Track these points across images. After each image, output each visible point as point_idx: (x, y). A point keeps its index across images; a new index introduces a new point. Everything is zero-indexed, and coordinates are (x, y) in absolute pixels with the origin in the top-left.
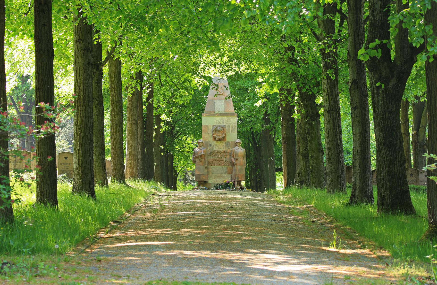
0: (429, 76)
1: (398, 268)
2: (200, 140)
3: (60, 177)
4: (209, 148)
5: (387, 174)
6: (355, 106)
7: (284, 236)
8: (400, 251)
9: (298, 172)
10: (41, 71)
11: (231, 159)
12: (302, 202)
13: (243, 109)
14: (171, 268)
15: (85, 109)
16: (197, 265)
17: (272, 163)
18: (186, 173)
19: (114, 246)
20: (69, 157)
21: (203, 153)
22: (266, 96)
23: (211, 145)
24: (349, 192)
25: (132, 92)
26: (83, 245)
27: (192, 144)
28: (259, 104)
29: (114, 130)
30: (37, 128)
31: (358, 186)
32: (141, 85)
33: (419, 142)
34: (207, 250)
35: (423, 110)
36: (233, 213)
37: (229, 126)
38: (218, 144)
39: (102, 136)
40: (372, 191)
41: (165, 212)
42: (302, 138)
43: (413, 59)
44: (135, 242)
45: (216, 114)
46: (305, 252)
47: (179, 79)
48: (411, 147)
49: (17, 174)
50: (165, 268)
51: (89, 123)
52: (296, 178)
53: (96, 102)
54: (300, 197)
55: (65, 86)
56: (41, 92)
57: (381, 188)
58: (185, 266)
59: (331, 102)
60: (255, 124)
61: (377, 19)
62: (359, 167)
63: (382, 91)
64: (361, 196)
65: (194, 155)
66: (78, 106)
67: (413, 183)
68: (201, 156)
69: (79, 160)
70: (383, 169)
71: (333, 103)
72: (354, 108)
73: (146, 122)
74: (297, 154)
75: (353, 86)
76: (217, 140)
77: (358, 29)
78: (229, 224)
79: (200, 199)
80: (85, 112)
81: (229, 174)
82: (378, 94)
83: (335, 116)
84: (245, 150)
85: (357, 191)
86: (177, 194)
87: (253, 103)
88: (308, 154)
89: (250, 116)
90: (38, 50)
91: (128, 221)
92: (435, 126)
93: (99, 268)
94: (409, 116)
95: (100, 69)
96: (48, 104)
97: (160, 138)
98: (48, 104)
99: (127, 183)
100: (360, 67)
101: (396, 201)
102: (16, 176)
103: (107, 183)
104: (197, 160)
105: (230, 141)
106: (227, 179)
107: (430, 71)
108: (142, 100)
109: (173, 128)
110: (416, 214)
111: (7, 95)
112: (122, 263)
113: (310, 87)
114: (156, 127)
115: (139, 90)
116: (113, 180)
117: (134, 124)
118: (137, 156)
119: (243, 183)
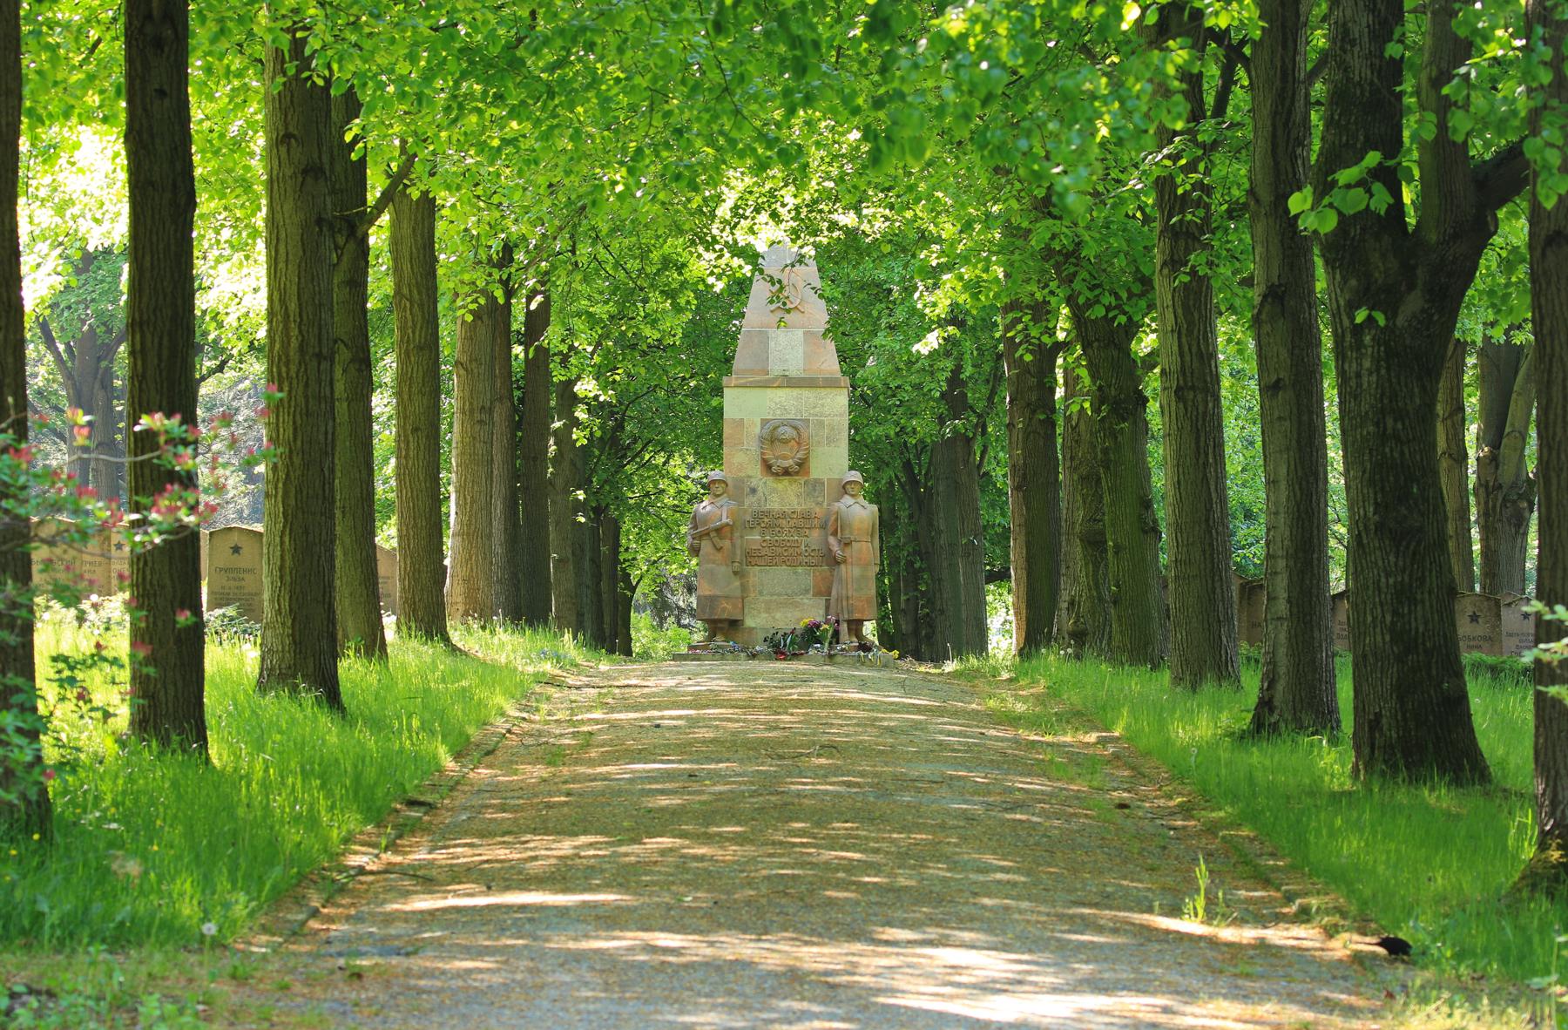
0: (1543, 301)
1: (1430, 1008)
2: (716, 474)
3: (212, 616)
4: (749, 501)
5: (1388, 638)
6: (1274, 378)
7: (1018, 871)
8: (1434, 941)
9: (1065, 597)
10: (148, 258)
11: (827, 543)
12: (1080, 718)
13: (870, 362)
14: (613, 1008)
15: (307, 385)
16: (706, 996)
17: (971, 552)
18: (667, 584)
19: (408, 908)
20: (248, 548)
21: (725, 520)
22: (955, 317)
23: (754, 491)
24: (1252, 683)
25: (474, 306)
26: (298, 903)
27: (687, 477)
28: (931, 342)
29: (407, 449)
30: (137, 508)
31: (1282, 670)
32: (505, 283)
33: (1500, 487)
35: (1516, 373)
36: (837, 771)
37: (821, 423)
38: (780, 486)
39: (364, 475)
40: (1333, 685)
41: (591, 763)
42: (1083, 479)
43: (1486, 223)
44: (481, 893)
45: (776, 379)
46: (1096, 939)
47: (644, 255)
48: (1472, 499)
49: (67, 673)
50: (591, 1007)
51: (321, 437)
52: (1064, 621)
53: (343, 355)
54: (1073, 698)
55: (235, 284)
56: (149, 336)
57: (1365, 688)
58: (666, 1000)
59: (1188, 358)
60: (914, 415)
61: (1357, 78)
62: (1289, 601)
63: (1373, 339)
64: (1293, 706)
65: (695, 527)
66: (279, 374)
67: (1479, 648)
68: (718, 530)
69: (282, 568)
70: (1374, 619)
71: (1196, 364)
72: (1270, 389)
73: (522, 404)
74: (1063, 530)
75: (1267, 307)
76: (777, 474)
77: (1287, 103)
78: (820, 815)
79: (716, 706)
80: (306, 397)
81: (818, 594)
82: (1358, 349)
83: (1201, 409)
84: (875, 508)
85: (1280, 686)
86: (633, 682)
87: (908, 342)
88: (1103, 534)
89: (898, 387)
90: (137, 181)
91: (460, 799)
92: (1563, 484)
93: (356, 1005)
94: (1467, 390)
95: (359, 234)
96: (176, 420)
97: (573, 463)
98: (176, 420)
99: (456, 637)
100: (1292, 238)
101: (1421, 735)
102: (60, 680)
103: (383, 645)
104: (706, 546)
105: (825, 477)
106: (812, 612)
107: (1549, 283)
108: (509, 325)
109: (620, 426)
110: (1490, 781)
111: (29, 322)
112: (438, 984)
113: (1118, 297)
114: (557, 425)
115: (501, 301)
116: (404, 628)
117: (481, 422)
118: (490, 536)
119: (869, 629)
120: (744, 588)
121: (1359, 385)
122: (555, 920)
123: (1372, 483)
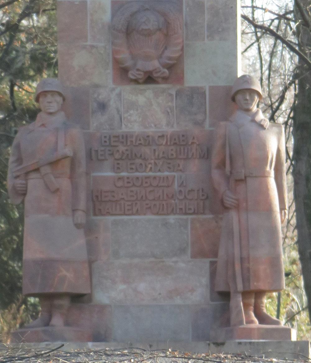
4: (97, 123)
38: (141, 100)
76: (136, 81)
81: (199, 254)
105: (205, 85)
120: (91, 248)
122: (147, 151)
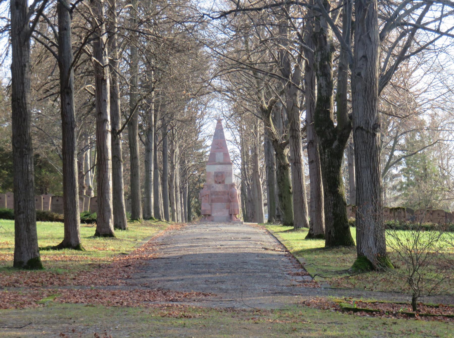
23: (213, 187)
34: (375, 63)
81: (227, 209)
120: (211, 208)
121: (325, 161)
123: (328, 181)
